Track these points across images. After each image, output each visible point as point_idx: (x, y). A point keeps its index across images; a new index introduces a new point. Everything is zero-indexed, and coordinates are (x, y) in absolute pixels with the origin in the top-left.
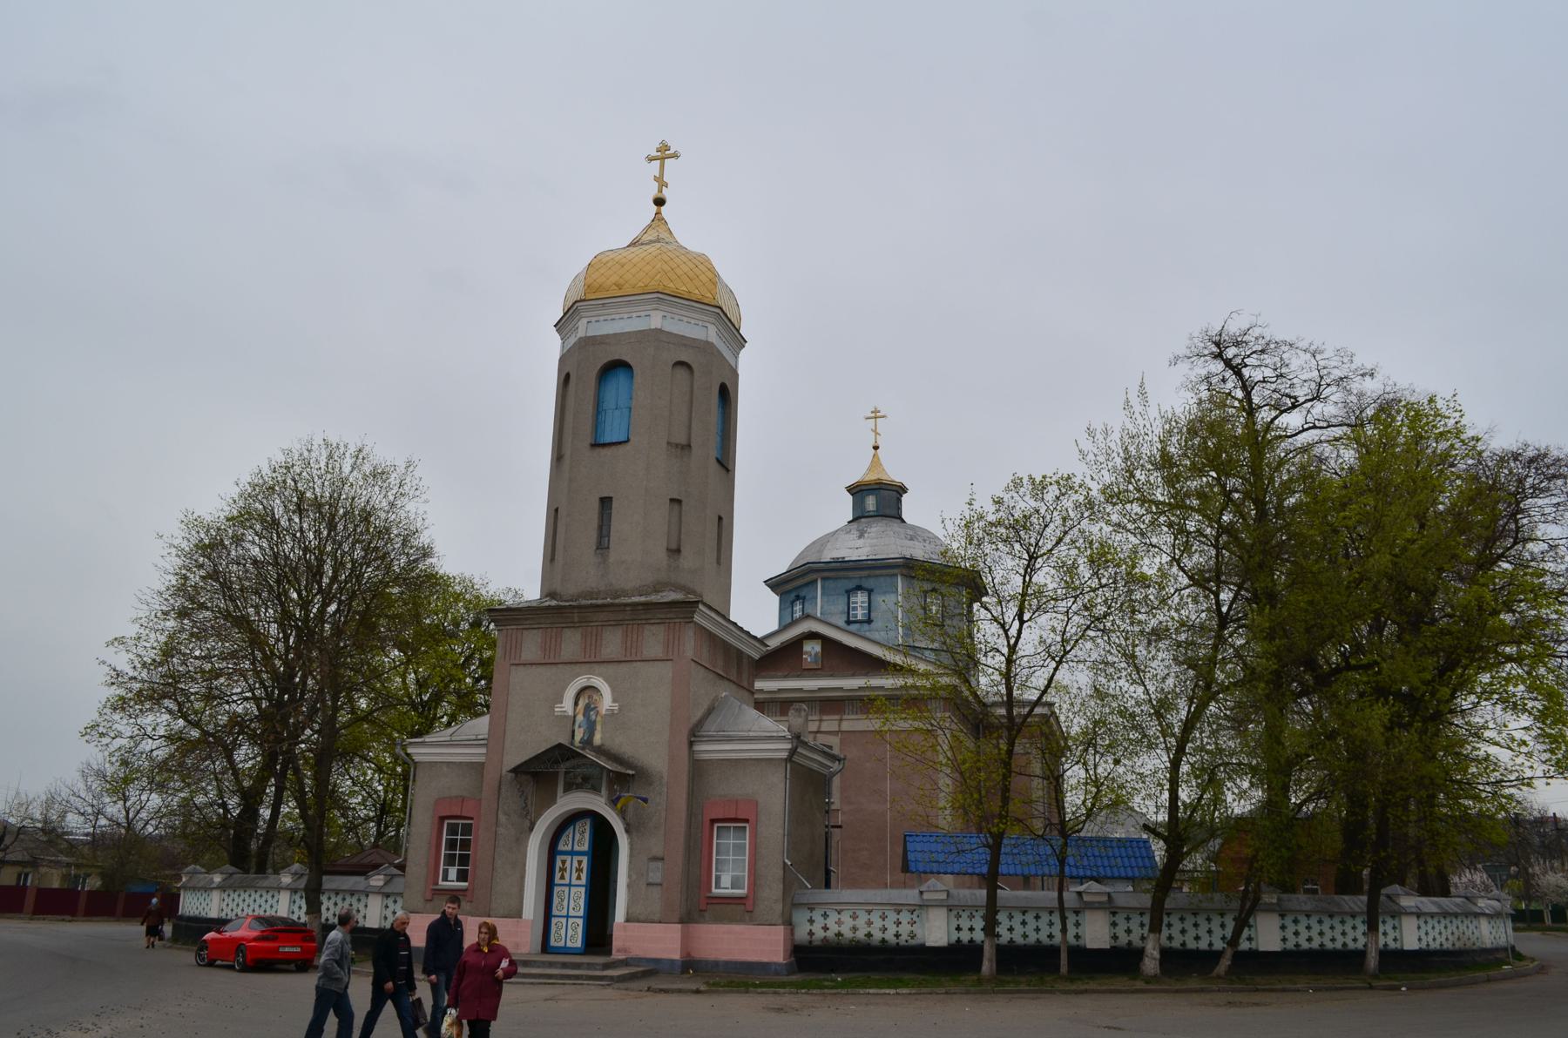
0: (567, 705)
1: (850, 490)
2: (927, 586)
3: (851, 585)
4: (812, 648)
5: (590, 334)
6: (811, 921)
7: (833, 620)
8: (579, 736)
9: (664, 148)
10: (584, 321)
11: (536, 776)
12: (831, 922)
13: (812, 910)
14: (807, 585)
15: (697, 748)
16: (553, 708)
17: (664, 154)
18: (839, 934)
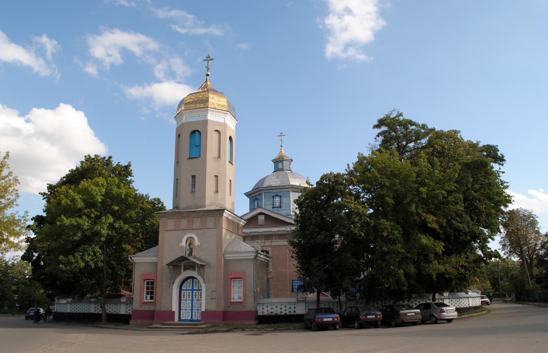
0: (184, 244)
1: (273, 161)
4: (261, 218)
5: (187, 121)
9: (208, 57)
11: (174, 266)
12: (269, 309)
13: (263, 305)
14: (259, 195)
15: (225, 256)
18: (272, 313)
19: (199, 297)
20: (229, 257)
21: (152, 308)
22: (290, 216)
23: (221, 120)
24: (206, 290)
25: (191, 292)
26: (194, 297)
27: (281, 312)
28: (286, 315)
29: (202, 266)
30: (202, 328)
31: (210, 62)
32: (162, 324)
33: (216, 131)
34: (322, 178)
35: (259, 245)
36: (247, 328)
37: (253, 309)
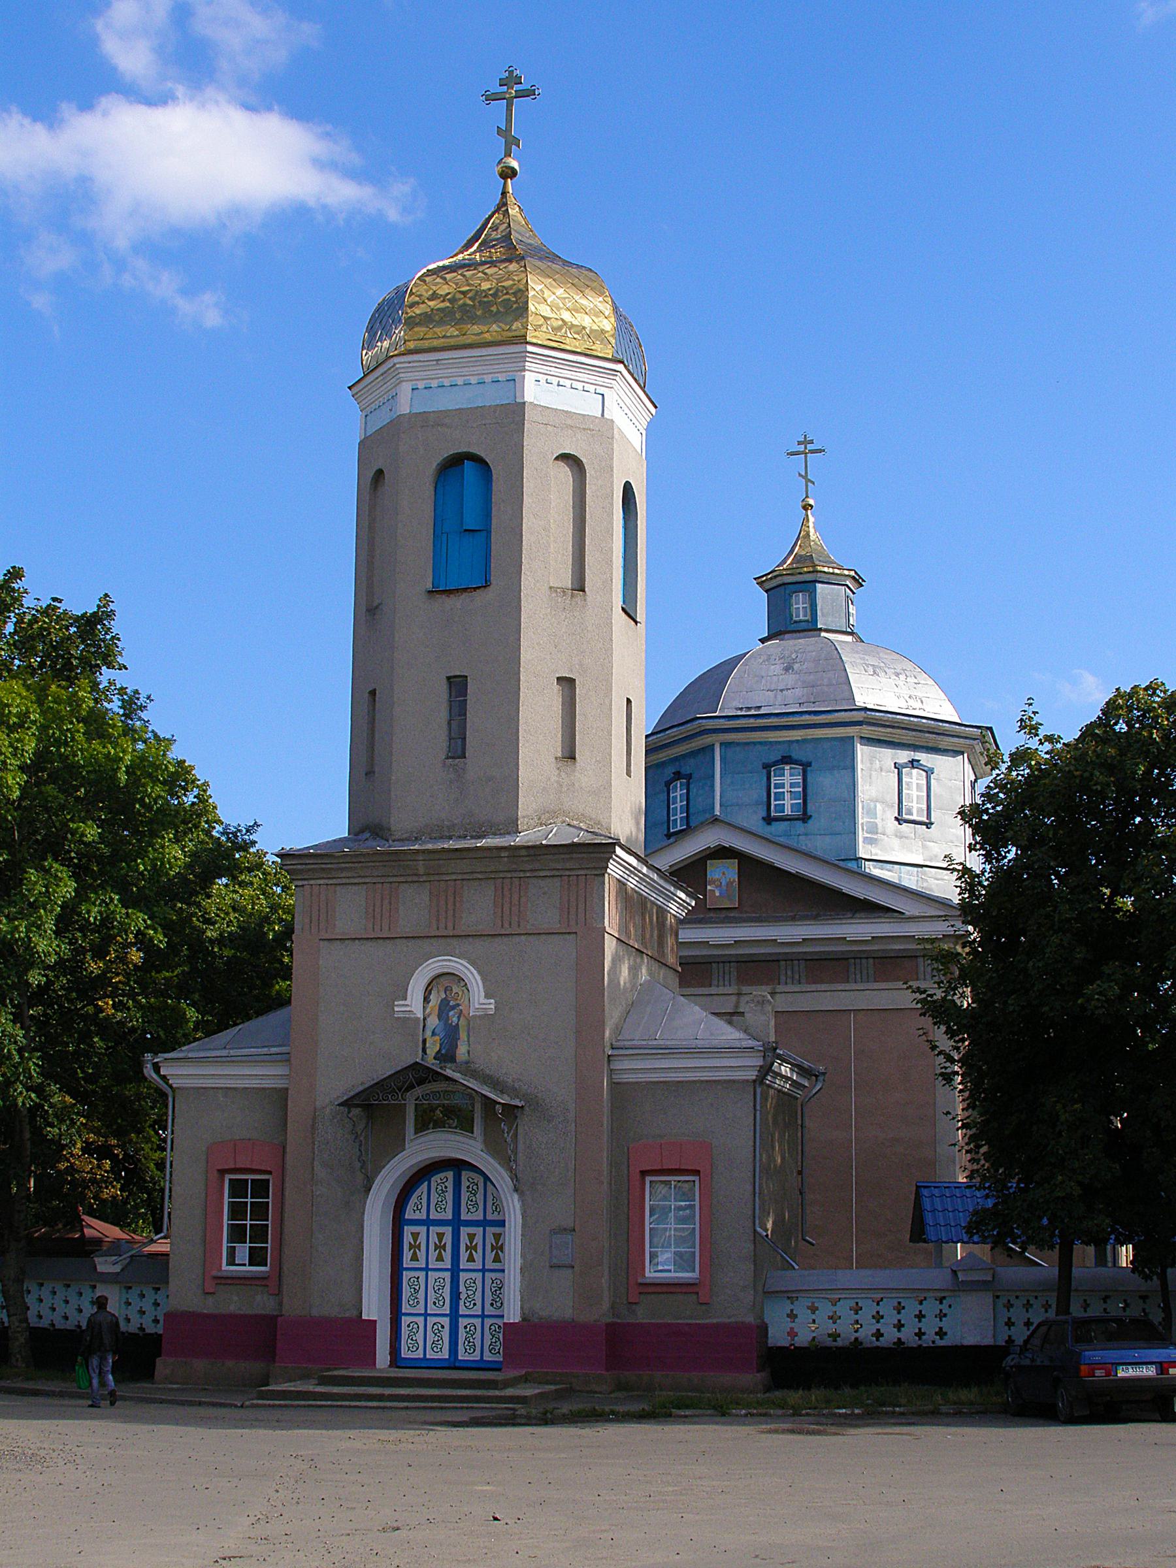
0: (414, 1003)
2: (904, 756)
3: (775, 756)
4: (723, 874)
6: (792, 1316)
7: (742, 820)
9: (511, 79)
10: (406, 388)
11: (368, 1108)
14: (693, 754)
15: (616, 1065)
17: (511, 89)
19: (490, 1256)
20: (633, 1069)
21: (261, 1303)
22: (852, 865)
23: (588, 406)
25: (448, 1231)
26: (464, 1255)
27: (878, 1334)
28: (920, 1352)
29: (511, 1111)
30: (522, 1400)
32: (323, 1381)
33: (565, 457)
34: (1110, 709)
35: (764, 1006)
36: (738, 1403)
37: (750, 1319)
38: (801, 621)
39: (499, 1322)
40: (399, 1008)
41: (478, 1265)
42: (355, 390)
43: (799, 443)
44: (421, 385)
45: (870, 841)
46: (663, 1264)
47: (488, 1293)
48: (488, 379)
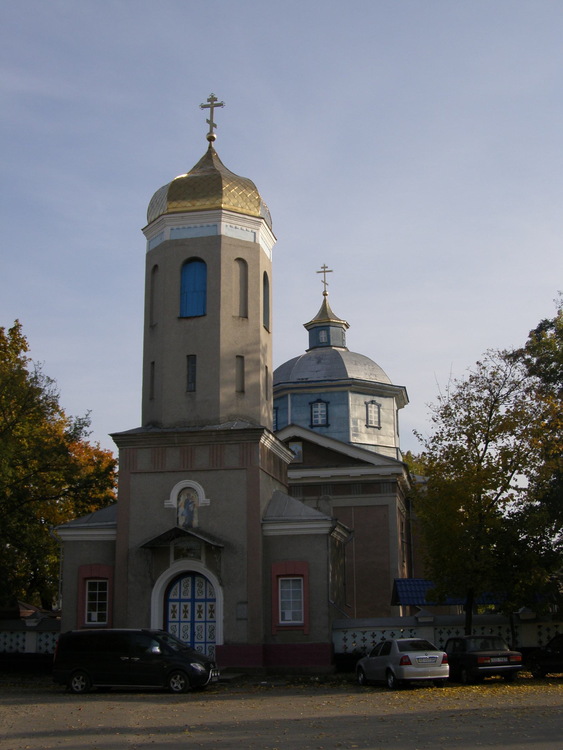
1: (307, 326)
2: (369, 398)
3: (314, 399)
6: (345, 640)
7: (301, 424)
8: (182, 522)
9: (212, 99)
10: (169, 228)
16: (163, 502)
17: (213, 103)
19: (209, 615)
24: (225, 601)
25: (189, 604)
26: (197, 615)
31: (215, 109)
33: (239, 260)
38: (323, 343)
39: (213, 645)
40: (167, 504)
41: (177, 619)
42: (145, 231)
43: (322, 268)
44: (175, 227)
45: (355, 435)
46: (290, 615)
47: (181, 631)
48: (205, 225)
